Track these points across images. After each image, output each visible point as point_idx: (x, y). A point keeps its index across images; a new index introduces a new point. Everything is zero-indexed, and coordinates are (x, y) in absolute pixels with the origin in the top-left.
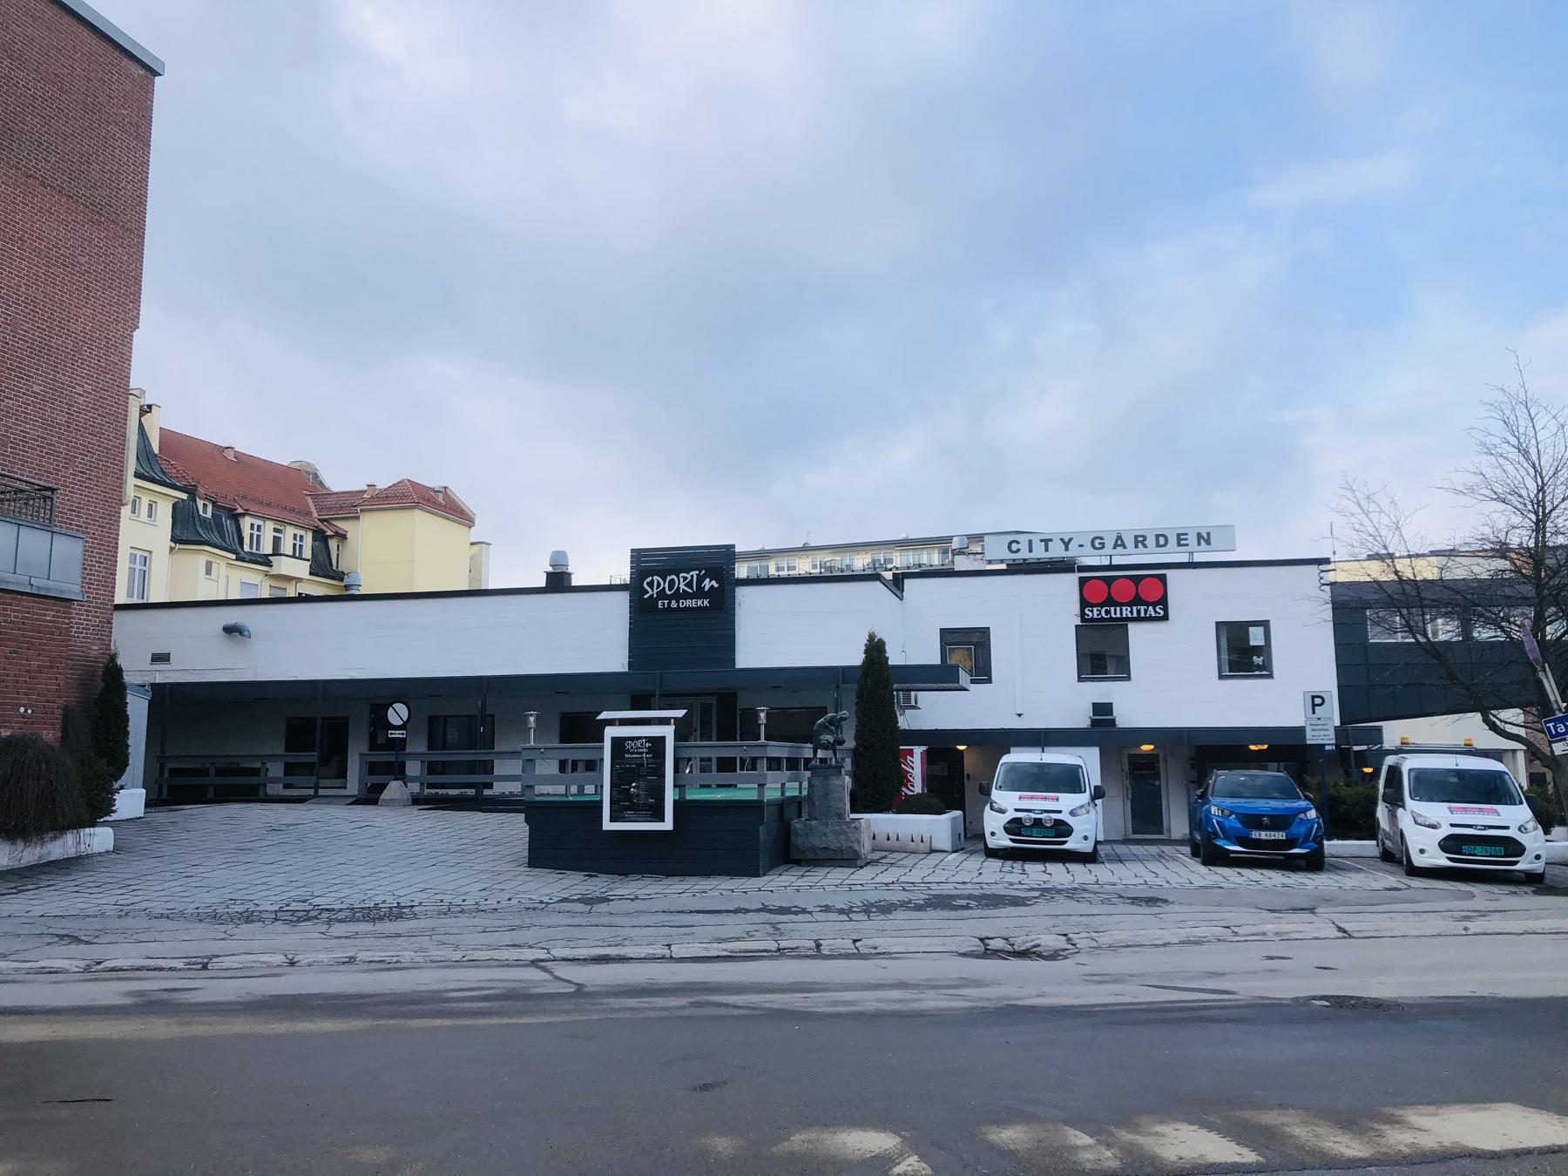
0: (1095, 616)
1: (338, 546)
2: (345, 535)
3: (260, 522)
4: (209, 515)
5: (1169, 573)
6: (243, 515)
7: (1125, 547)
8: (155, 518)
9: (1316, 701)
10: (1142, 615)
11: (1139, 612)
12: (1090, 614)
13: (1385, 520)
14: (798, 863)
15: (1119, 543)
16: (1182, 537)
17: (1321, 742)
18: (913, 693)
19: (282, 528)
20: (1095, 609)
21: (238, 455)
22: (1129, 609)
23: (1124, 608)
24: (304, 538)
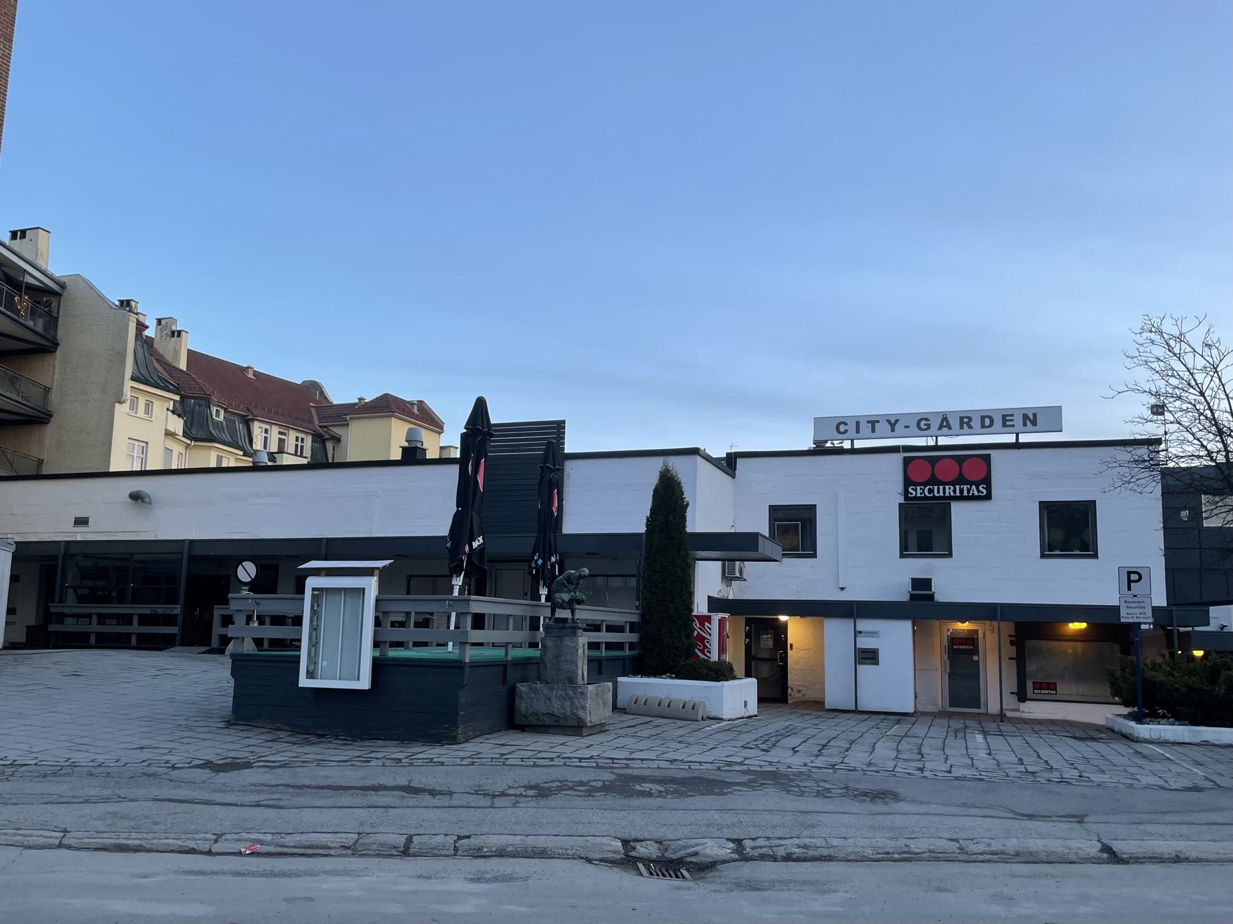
0: (919, 495)
1: (334, 447)
2: (340, 439)
3: (268, 427)
4: (221, 418)
5: (994, 454)
6: (253, 420)
7: (950, 428)
8: (152, 413)
9: (1133, 577)
10: (965, 494)
11: (962, 491)
12: (914, 493)
13: (1200, 363)
14: (522, 728)
15: (945, 424)
16: (1008, 418)
17: (1136, 620)
18: (737, 563)
19: (286, 432)
20: (918, 488)
21: (256, 373)
22: (952, 488)
23: (947, 487)
24: (305, 440)
